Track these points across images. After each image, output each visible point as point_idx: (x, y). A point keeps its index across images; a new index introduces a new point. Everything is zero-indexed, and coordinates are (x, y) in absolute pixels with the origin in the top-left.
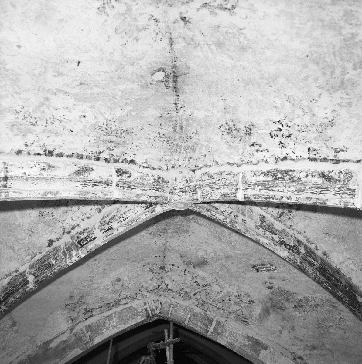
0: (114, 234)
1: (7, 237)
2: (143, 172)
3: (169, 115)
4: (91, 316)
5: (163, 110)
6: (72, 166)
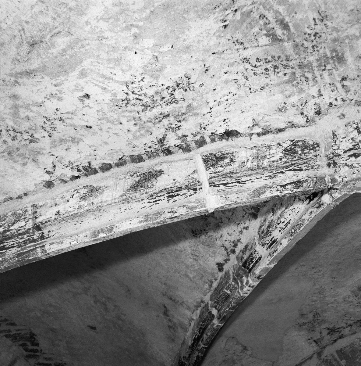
0: (278, 251)
1: (178, 265)
2: (257, 146)
3: (238, 13)
4: (340, 338)
5: (218, 10)
6: (128, 177)
